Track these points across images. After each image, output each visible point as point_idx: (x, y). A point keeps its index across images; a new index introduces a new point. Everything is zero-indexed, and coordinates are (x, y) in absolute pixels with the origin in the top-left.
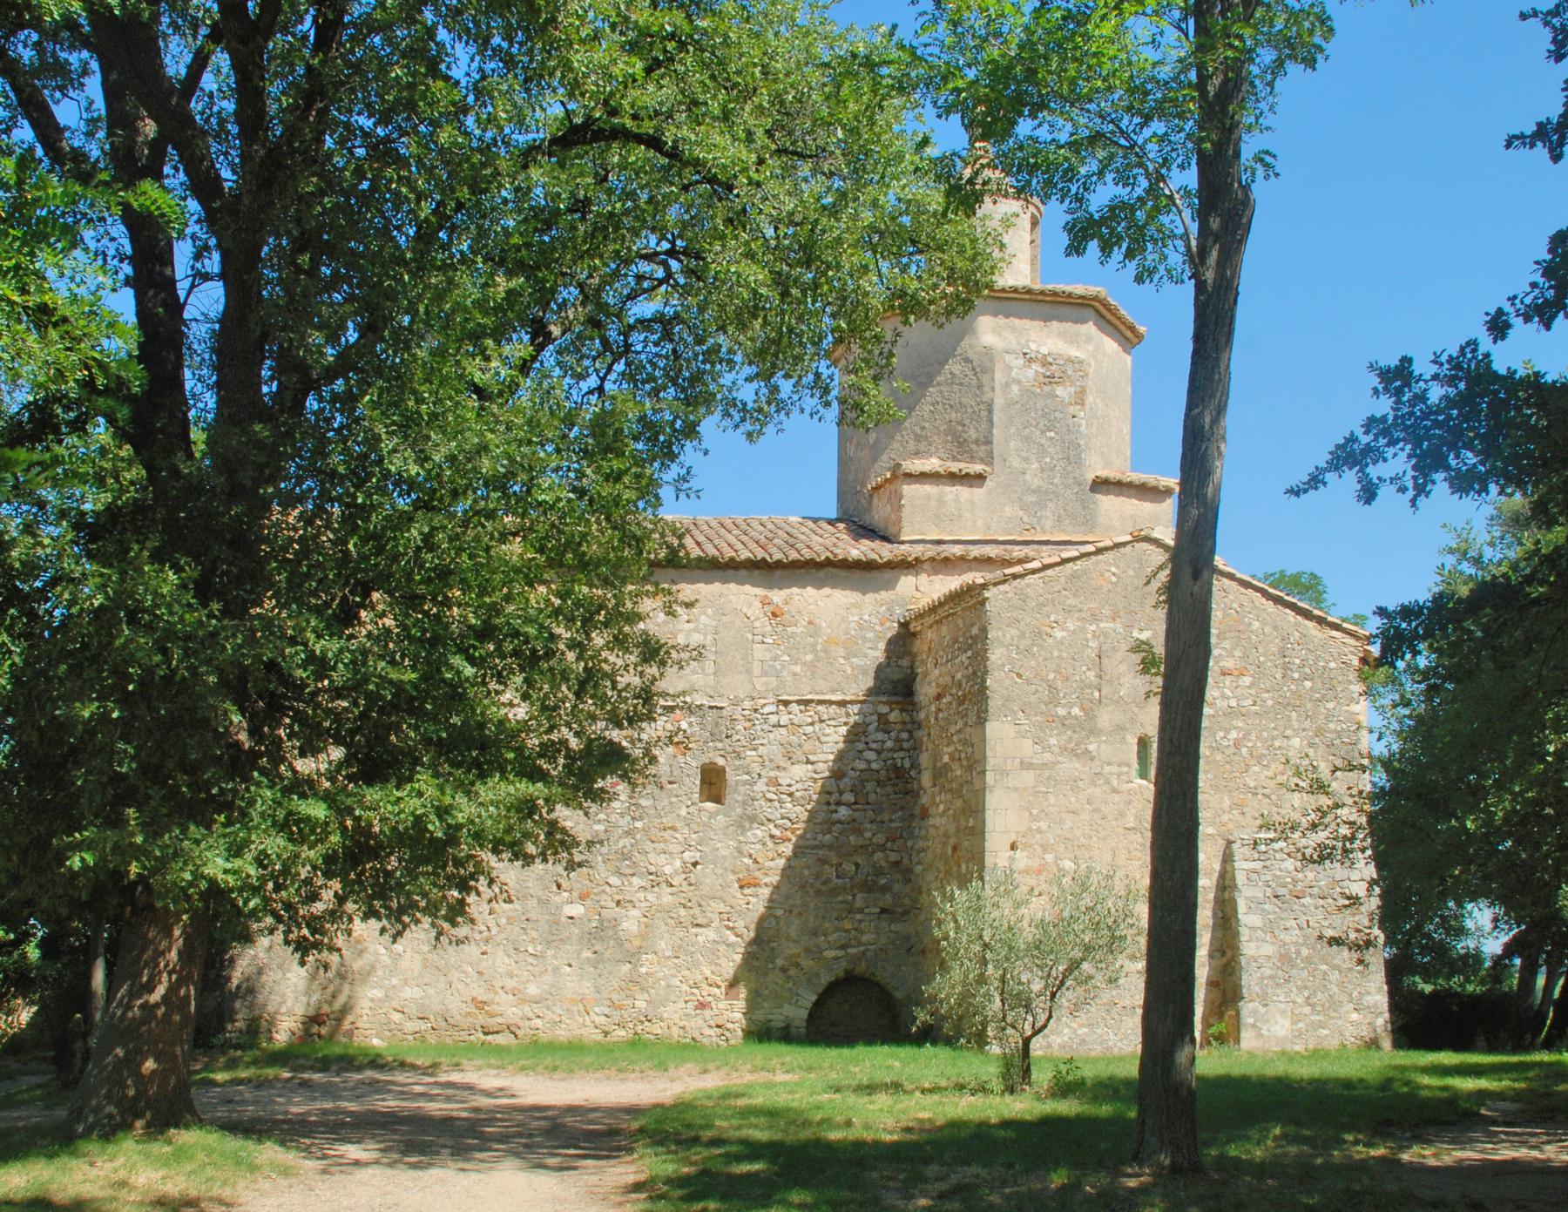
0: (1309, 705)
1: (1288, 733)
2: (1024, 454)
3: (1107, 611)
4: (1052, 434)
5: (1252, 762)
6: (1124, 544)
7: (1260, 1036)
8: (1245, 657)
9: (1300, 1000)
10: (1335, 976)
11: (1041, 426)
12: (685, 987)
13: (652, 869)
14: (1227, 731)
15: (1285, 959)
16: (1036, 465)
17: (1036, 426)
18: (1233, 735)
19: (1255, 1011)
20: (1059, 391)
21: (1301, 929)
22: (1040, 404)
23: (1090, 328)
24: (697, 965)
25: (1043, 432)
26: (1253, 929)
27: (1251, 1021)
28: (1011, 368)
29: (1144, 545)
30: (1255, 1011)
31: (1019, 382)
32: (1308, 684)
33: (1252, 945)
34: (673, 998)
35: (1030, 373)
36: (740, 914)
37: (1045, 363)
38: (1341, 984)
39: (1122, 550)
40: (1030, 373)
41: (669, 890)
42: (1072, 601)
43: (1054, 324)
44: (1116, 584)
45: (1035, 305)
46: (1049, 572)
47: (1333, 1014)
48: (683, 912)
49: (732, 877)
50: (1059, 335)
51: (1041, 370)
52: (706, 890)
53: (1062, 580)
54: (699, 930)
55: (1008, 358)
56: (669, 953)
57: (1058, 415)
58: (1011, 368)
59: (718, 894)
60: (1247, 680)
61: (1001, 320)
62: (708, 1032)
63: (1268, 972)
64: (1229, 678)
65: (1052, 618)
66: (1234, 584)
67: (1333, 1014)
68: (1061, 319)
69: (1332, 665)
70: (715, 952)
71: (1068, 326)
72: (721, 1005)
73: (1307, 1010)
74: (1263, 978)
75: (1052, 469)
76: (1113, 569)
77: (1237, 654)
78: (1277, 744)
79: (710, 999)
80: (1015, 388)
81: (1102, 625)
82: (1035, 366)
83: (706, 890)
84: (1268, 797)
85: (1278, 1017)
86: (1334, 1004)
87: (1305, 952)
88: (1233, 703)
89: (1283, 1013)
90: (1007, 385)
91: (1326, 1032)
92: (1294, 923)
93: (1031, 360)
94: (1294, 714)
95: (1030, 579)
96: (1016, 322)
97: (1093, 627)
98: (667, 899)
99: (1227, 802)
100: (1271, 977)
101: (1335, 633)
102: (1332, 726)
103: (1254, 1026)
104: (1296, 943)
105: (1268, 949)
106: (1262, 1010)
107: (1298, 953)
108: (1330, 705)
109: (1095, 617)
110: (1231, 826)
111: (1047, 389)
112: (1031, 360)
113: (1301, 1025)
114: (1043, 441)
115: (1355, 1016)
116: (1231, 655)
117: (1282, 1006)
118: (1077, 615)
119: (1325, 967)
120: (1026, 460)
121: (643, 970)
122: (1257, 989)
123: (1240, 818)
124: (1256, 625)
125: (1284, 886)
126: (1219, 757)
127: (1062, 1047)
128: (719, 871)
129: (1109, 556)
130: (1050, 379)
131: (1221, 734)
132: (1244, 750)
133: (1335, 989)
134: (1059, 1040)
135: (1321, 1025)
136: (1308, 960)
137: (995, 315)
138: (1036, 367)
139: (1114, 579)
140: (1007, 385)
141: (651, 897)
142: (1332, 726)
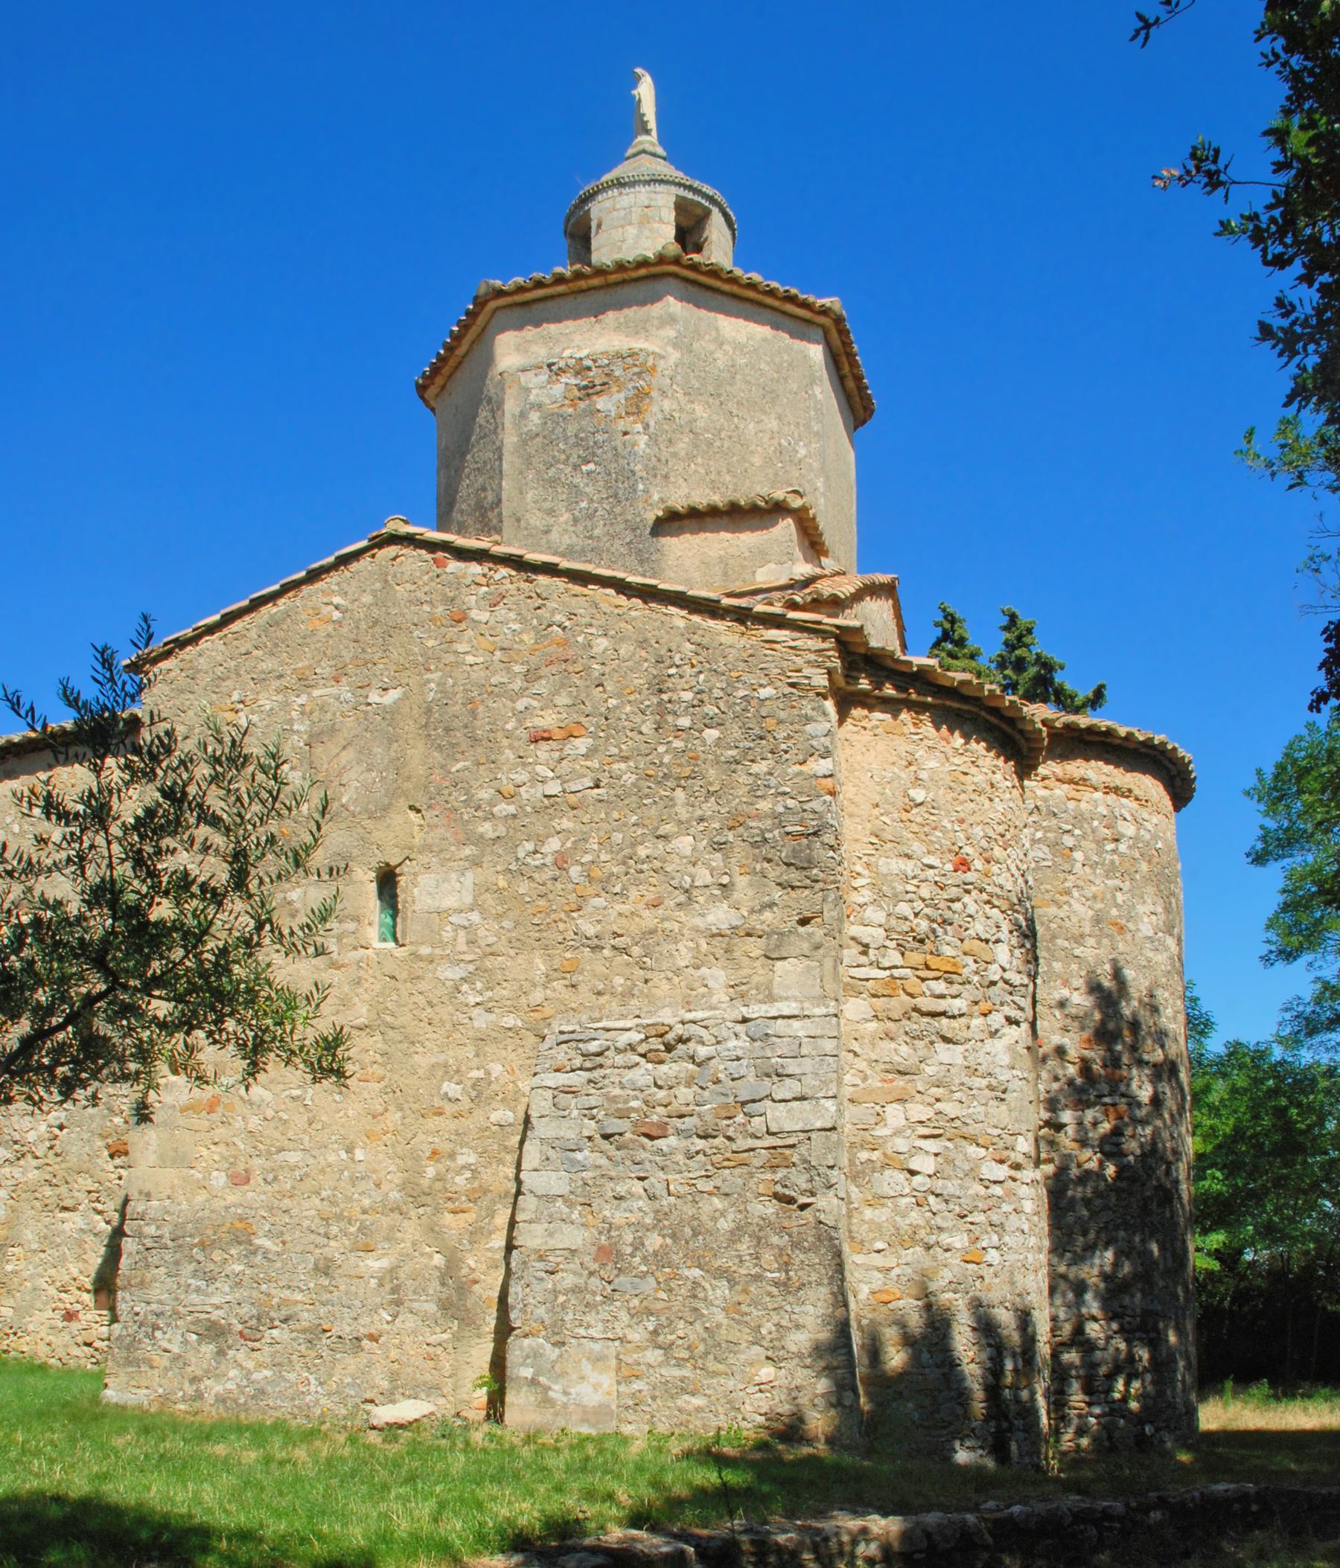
0: (712, 773)
1: (665, 829)
2: (547, 505)
3: (325, 669)
4: (591, 466)
5: (590, 890)
6: (356, 555)
7: (546, 1402)
8: (577, 703)
9: (636, 1335)
10: (720, 1291)
11: (574, 459)
12: (52, 1291)
13: (17, 1137)
14: (541, 840)
15: (608, 1254)
16: (566, 517)
17: (566, 462)
18: (554, 844)
19: (536, 1354)
20: (601, 403)
21: (652, 1197)
22: (571, 430)
23: (672, 305)
24: (63, 1259)
25: (576, 467)
26: (549, 1198)
27: (527, 1372)
28: (528, 390)
29: (392, 550)
30: (536, 1354)
31: (539, 406)
32: (710, 735)
33: (539, 1229)
34: (39, 1305)
35: (558, 389)
36: (110, 1193)
37: (581, 370)
38: (733, 1309)
39: (355, 566)
40: (558, 389)
41: (35, 1163)
42: (268, 664)
43: (611, 316)
44: (340, 623)
45: (580, 298)
46: (237, 626)
47: (712, 1365)
48: (48, 1191)
49: (100, 1143)
50: (618, 329)
51: (574, 381)
52: (73, 1160)
53: (253, 634)
54: (66, 1215)
55: (526, 379)
56: (35, 1246)
57: (599, 437)
58: (528, 390)
59: (85, 1166)
60: (582, 745)
61: (530, 332)
62: (76, 1351)
63: (567, 1280)
64: (544, 746)
65: (236, 697)
66: (560, 583)
67: (712, 1365)
68: (619, 306)
69: (765, 692)
70: (80, 1243)
71: (631, 313)
72: (89, 1317)
73: (653, 1356)
74: (555, 1292)
75: (591, 517)
76: (337, 600)
77: (562, 700)
78: (642, 852)
79: (78, 1307)
80: (535, 417)
81: (316, 693)
82: (564, 379)
83: (73, 1160)
84: (624, 951)
85: (587, 1368)
86: (716, 1347)
87: (654, 1241)
88: (553, 788)
89: (598, 1359)
90: (523, 415)
91: (698, 1401)
92: (638, 1187)
93: (562, 371)
94: (680, 794)
95: (205, 643)
96: (552, 328)
97: (302, 699)
98: (33, 1175)
99: (541, 966)
100: (576, 1290)
101: (773, 634)
102: (764, 806)
103: (533, 1382)
104: (637, 1226)
105: (574, 1237)
106: (552, 1353)
107: (638, 1245)
108: (760, 768)
109: (305, 683)
110: (548, 1011)
111: (582, 405)
112: (562, 371)
113: (637, 1385)
114: (577, 480)
115: (767, 1372)
116: (549, 704)
117: (597, 1347)
118: (276, 684)
119: (696, 1273)
120: (551, 512)
121: (9, 1268)
122: (541, 1311)
123: (566, 994)
124: (602, 644)
125: (623, 1115)
126: (524, 887)
127: (221, 1400)
128: (86, 1136)
129: (332, 580)
130: (588, 391)
131: (530, 846)
132: (575, 871)
133: (720, 1317)
134: (219, 1388)
135: (685, 1388)
136: (660, 1259)
137: (520, 327)
138: (569, 379)
139: (337, 615)
140: (523, 415)
141: (17, 1172)
142: (764, 806)
